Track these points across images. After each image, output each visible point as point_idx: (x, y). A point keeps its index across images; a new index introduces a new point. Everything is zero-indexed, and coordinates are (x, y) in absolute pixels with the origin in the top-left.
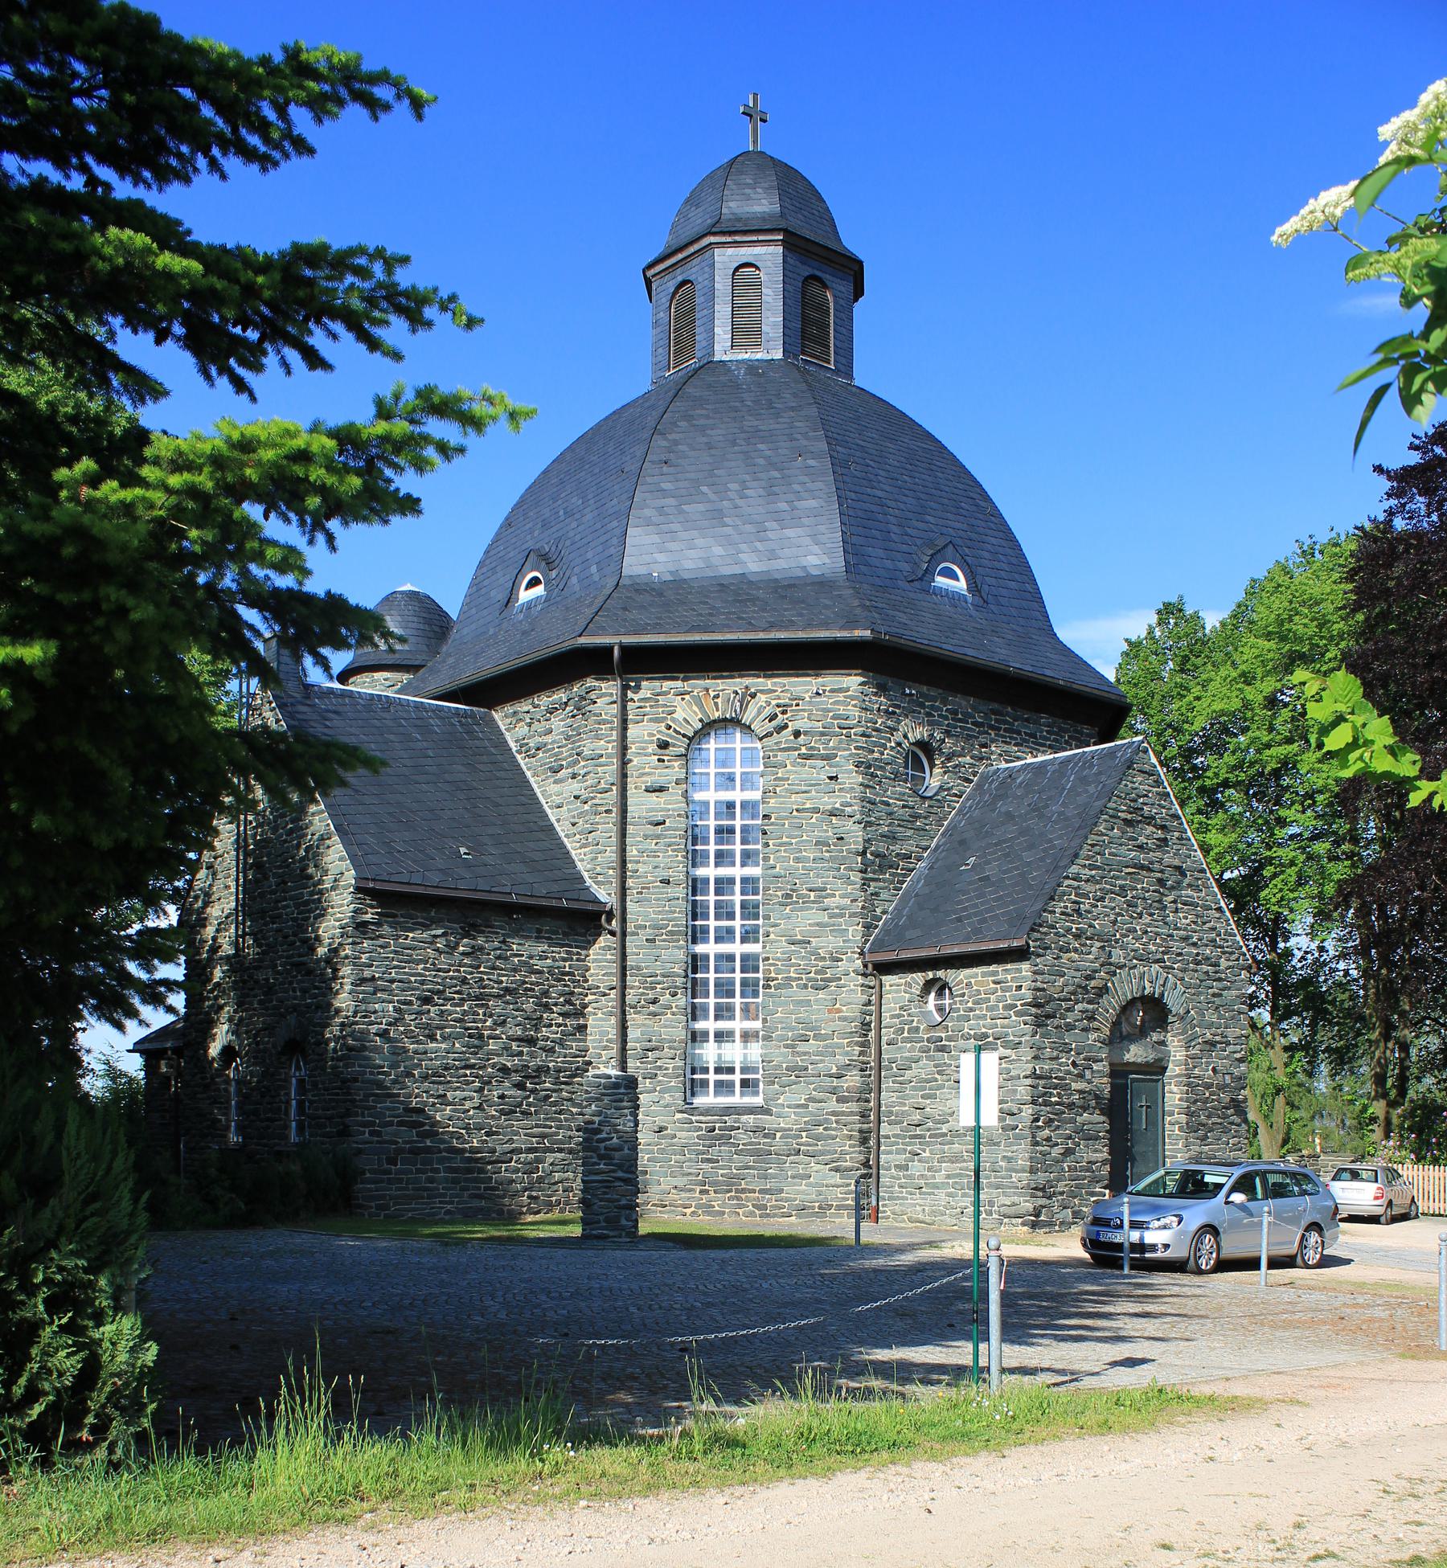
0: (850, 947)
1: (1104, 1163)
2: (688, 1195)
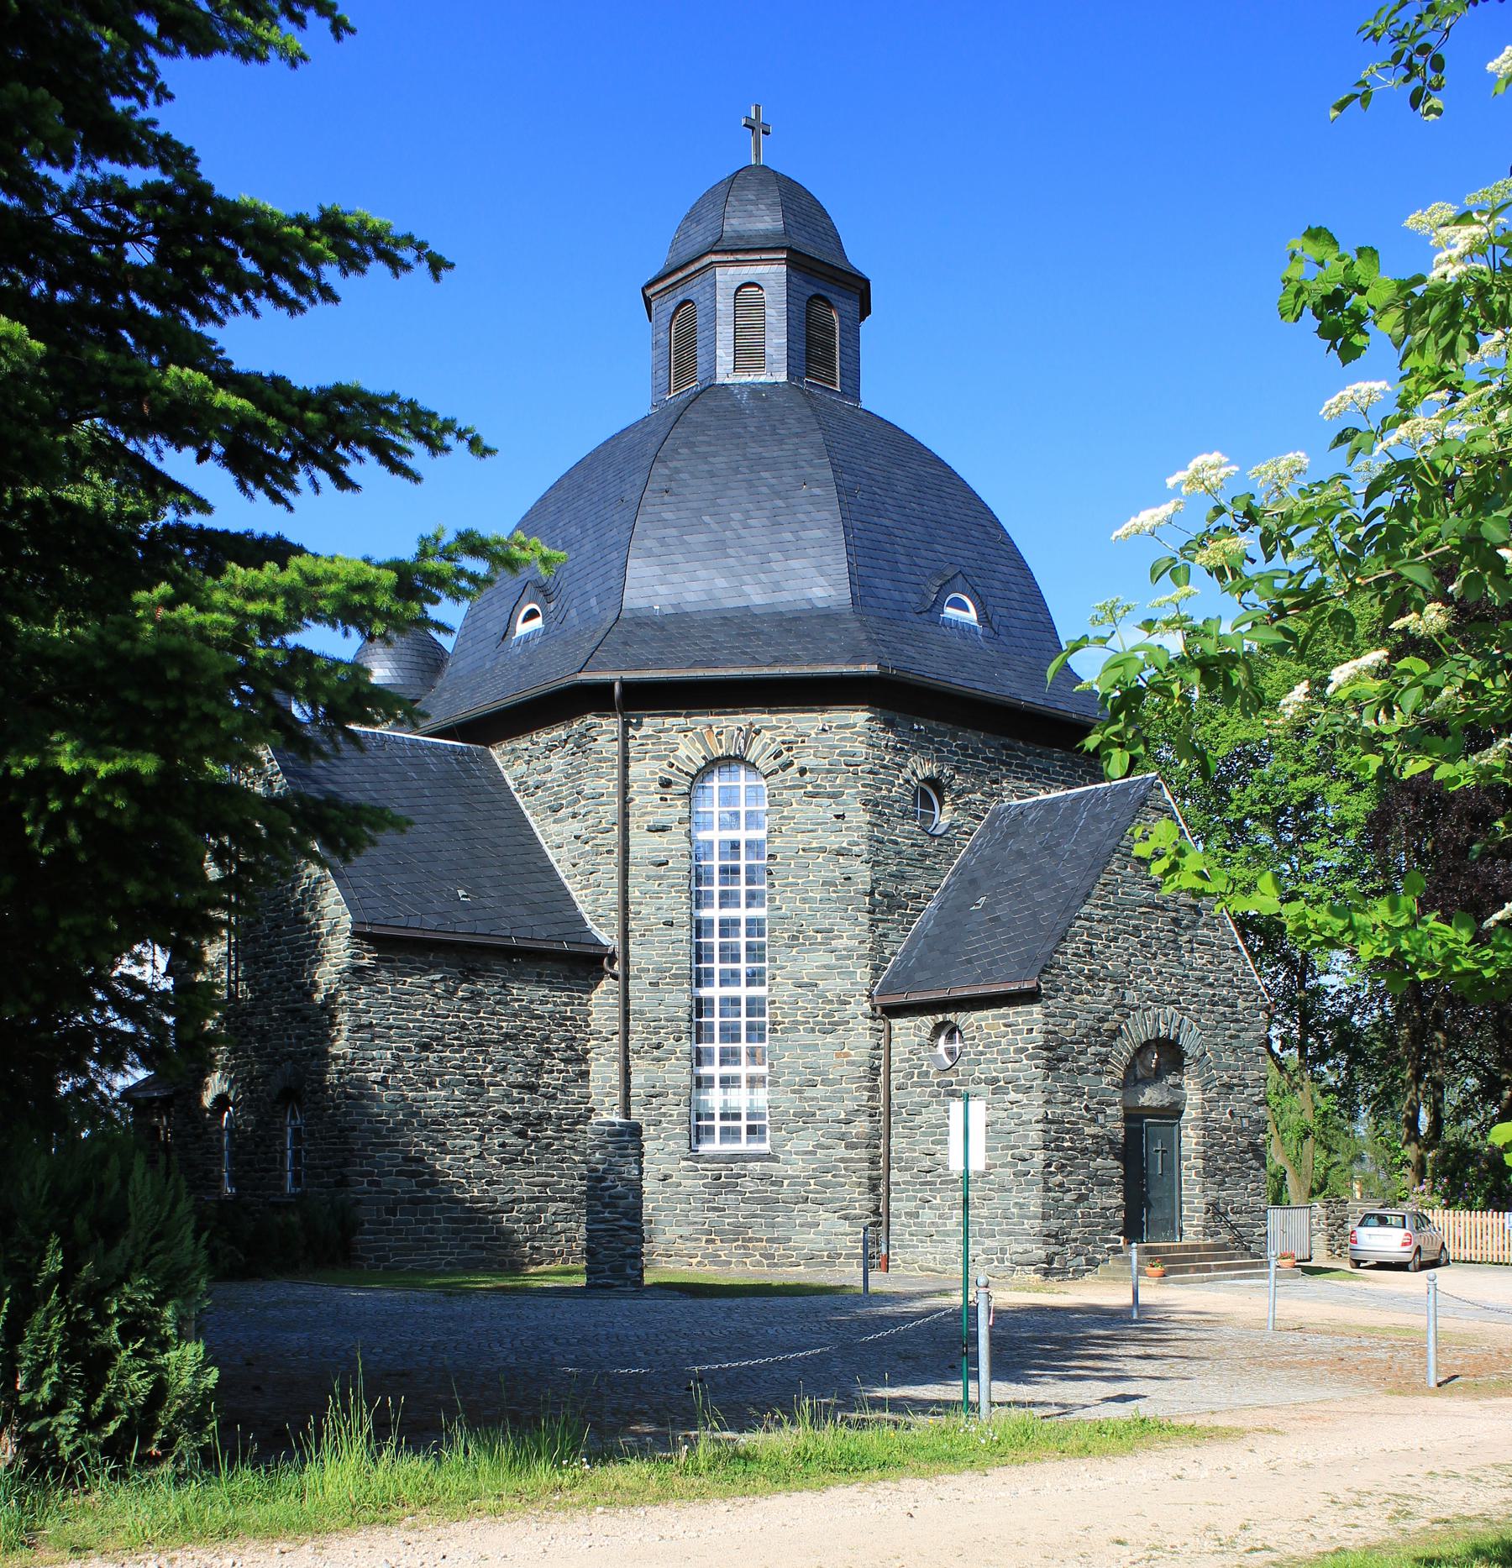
0: (858, 990)
1: (1118, 1208)
2: (693, 1244)
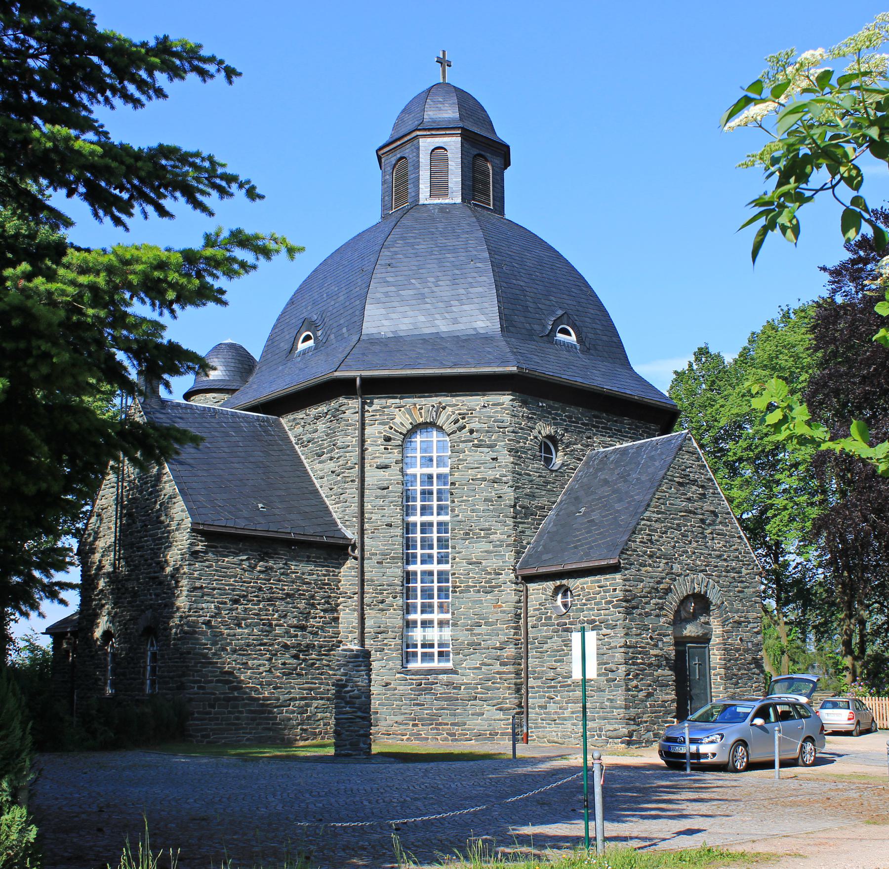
1: (673, 701)
2: (404, 727)
